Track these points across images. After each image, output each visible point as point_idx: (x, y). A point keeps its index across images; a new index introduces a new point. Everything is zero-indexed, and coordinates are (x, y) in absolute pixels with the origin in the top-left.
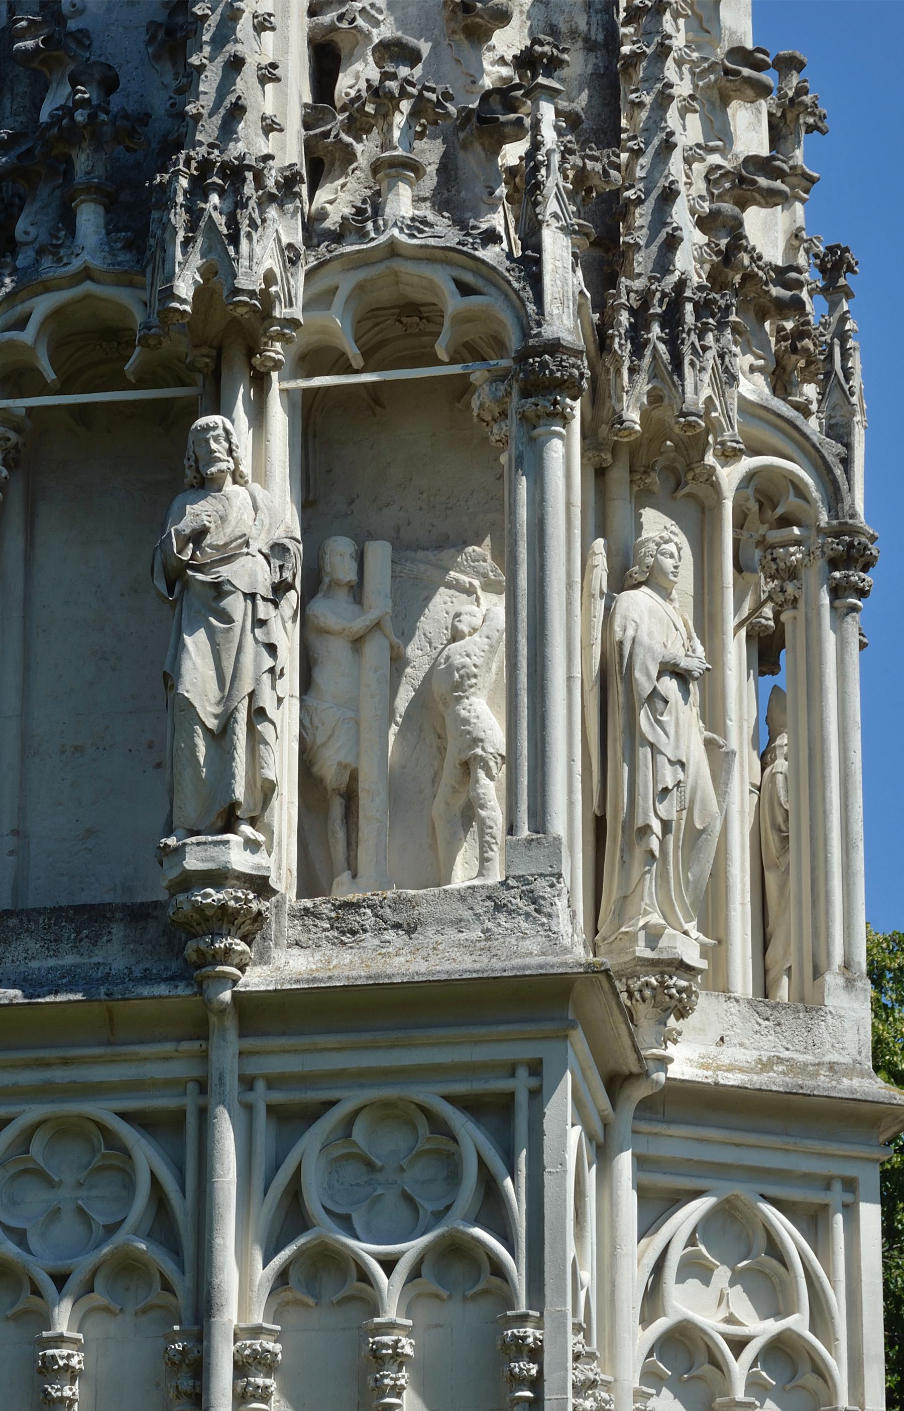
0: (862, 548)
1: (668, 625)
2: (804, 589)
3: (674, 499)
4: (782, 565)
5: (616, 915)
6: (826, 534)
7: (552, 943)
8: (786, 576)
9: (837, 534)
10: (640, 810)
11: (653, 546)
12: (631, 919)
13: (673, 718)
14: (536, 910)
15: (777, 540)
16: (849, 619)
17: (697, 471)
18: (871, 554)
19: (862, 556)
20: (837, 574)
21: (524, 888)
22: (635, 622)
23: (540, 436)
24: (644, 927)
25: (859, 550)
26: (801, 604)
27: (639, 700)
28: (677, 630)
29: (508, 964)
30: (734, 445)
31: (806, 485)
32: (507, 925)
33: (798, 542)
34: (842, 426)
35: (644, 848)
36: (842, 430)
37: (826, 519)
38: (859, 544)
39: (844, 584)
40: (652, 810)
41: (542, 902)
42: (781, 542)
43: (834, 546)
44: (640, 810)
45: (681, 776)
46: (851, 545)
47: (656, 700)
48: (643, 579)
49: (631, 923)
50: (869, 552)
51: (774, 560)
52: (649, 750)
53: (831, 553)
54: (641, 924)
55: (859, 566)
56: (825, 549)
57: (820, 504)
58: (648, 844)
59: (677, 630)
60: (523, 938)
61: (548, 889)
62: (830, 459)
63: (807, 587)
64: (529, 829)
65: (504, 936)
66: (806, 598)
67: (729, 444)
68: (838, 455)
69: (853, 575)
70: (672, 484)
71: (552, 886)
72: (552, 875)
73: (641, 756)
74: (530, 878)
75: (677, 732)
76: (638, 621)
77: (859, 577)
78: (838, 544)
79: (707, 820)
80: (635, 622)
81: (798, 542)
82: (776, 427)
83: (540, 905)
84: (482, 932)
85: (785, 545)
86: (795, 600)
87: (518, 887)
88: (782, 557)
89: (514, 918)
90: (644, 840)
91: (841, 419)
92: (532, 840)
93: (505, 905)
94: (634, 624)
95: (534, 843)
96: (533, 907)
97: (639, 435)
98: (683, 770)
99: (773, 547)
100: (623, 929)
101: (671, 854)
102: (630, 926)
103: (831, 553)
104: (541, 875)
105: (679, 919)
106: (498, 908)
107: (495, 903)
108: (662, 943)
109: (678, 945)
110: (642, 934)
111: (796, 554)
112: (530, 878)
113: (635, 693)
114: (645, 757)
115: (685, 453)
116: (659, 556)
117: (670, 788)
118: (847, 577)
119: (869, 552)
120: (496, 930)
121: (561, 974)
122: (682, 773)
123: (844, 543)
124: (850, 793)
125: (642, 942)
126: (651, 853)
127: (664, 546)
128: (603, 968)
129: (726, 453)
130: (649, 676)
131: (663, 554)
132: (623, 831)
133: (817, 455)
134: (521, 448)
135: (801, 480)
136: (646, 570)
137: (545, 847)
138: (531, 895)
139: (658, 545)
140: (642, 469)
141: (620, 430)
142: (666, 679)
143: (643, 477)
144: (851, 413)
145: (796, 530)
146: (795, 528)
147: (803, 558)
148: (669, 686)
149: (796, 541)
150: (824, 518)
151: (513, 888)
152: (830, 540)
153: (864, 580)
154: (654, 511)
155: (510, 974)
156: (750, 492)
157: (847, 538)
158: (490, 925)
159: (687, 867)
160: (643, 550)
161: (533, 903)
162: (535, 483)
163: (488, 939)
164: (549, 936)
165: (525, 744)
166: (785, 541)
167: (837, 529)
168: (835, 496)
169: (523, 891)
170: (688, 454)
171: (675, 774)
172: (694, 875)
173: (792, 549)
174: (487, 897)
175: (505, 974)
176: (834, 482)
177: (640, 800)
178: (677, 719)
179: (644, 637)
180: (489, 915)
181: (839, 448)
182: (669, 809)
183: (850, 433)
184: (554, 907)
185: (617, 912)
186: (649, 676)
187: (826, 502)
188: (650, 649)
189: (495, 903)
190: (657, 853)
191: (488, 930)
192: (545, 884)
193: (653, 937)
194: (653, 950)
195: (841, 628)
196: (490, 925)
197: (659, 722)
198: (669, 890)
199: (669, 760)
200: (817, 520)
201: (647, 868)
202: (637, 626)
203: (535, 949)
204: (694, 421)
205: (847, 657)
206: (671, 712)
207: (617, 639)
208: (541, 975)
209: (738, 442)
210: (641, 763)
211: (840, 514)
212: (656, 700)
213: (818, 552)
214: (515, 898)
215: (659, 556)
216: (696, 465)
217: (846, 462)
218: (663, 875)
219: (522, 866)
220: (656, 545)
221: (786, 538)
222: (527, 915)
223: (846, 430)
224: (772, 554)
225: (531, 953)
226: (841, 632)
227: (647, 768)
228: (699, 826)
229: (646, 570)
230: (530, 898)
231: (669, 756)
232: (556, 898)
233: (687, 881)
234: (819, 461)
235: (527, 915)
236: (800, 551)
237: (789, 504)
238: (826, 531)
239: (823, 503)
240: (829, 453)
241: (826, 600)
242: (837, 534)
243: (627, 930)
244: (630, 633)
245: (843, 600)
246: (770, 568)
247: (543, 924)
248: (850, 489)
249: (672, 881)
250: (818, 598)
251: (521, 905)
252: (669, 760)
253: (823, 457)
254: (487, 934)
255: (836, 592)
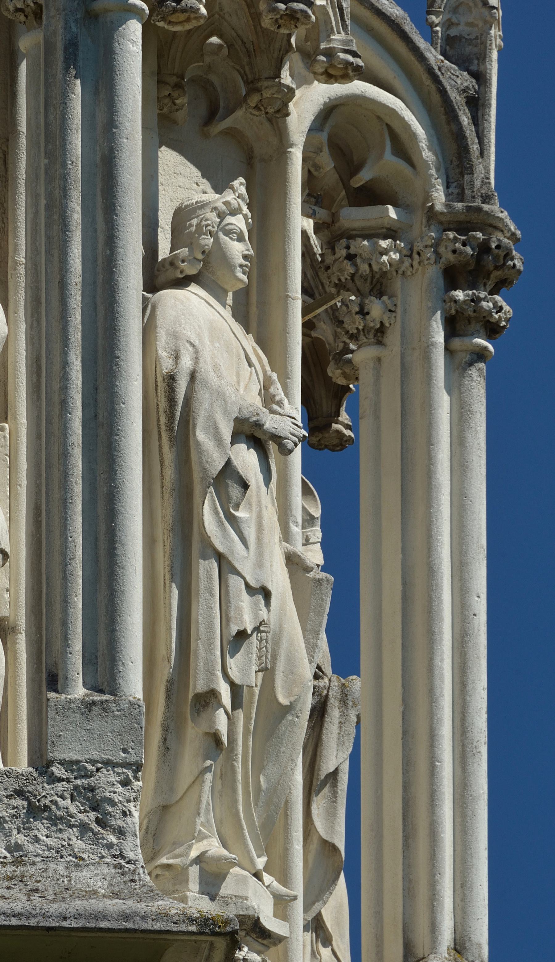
0: (502, 253)
1: (238, 356)
2: (399, 311)
3: (206, 136)
4: (364, 268)
5: (150, 836)
6: (441, 223)
7: (127, 878)
8: (366, 288)
9: (463, 227)
10: (199, 667)
11: (213, 217)
12: (176, 844)
13: (254, 515)
14: (98, 821)
15: (357, 225)
16: (474, 372)
17: (267, 94)
18: (514, 265)
19: (497, 268)
20: (460, 295)
21: (79, 782)
22: (192, 345)
23: (106, 11)
24: (199, 860)
25: (496, 258)
26: (393, 338)
27: (203, 479)
28: (250, 365)
29: (54, 908)
30: (350, 58)
31: (414, 136)
32: (49, 841)
33: (391, 233)
34: (470, 42)
35: (204, 727)
36: (469, 49)
37: (443, 198)
38: (498, 247)
39: (470, 312)
40: (220, 668)
41: (110, 809)
42: (363, 229)
43: (458, 245)
44: (201, 665)
45: (264, 614)
46: (484, 248)
47: (229, 482)
48: (192, 271)
49: (177, 851)
50: (510, 263)
51: (351, 257)
52: (215, 565)
53: (451, 257)
54: (194, 854)
55: (490, 285)
56: (442, 250)
57: (433, 171)
58: (212, 722)
59: (250, 365)
60: (77, 866)
61: (119, 788)
62: (455, 97)
63: (405, 311)
64: (85, 685)
65: (45, 859)
66: (403, 328)
67: (342, 55)
68: (464, 91)
69: (485, 299)
70: (203, 110)
71: (125, 783)
72: (126, 765)
73: (202, 574)
74: (89, 767)
75: (259, 540)
76: (197, 343)
77: (495, 303)
78: (464, 244)
79: (296, 691)
80: (192, 345)
81: (391, 233)
82: (370, 31)
83: (106, 814)
84: (8, 849)
85: (372, 234)
86: (381, 331)
87: (68, 780)
88: (365, 255)
89: (61, 831)
90: (204, 715)
91: (468, 29)
92: (94, 703)
93: (46, 808)
94: (191, 349)
95: (96, 709)
96: (92, 815)
97: (202, 21)
98: (268, 603)
99: (350, 235)
100: (164, 860)
101: (240, 742)
102: (176, 857)
103: (451, 257)
104: (108, 763)
105: (249, 852)
106: (36, 811)
107: (30, 803)
108: (227, 889)
109: (250, 894)
110: (194, 872)
111: (390, 252)
112: (89, 767)
113: (195, 467)
114: (210, 577)
115: (246, 60)
116: (221, 234)
117: (249, 632)
118: (476, 300)
119: (510, 263)
120: (31, 848)
121: (160, 932)
122: (264, 609)
123: (475, 243)
124: (470, 664)
125: (194, 885)
126: (216, 738)
127: (229, 219)
128: (229, 929)
129: (331, 71)
130: (218, 440)
131: (227, 233)
132: (168, 697)
133: (433, 88)
134: (74, 29)
135: (407, 126)
136: (200, 257)
137: (114, 717)
138: (90, 794)
139: (221, 216)
140: (174, 79)
141: (175, 10)
142: (242, 447)
143: (175, 94)
144: (486, 22)
145: (392, 213)
146: (390, 207)
147: (401, 261)
148: (246, 459)
149: (389, 229)
150: (439, 197)
151: (60, 780)
152: (451, 234)
153: (501, 308)
154: (174, 154)
155: (74, 925)
156: (323, 137)
157: (479, 235)
158: (21, 839)
159: (259, 768)
160: (195, 222)
161: (94, 809)
162: (96, 92)
163: (18, 862)
164: (121, 867)
165: (79, 539)
166: (370, 228)
167: (462, 218)
168: (458, 162)
169: (76, 788)
170: (250, 63)
171: (255, 609)
172: (268, 781)
173: (384, 244)
174: (15, 791)
175: (66, 924)
176: (459, 136)
177: (199, 647)
178: (260, 517)
179: (207, 370)
180: (18, 822)
181: (465, 80)
182: (243, 667)
183: (483, 57)
184: (128, 819)
185: (152, 830)
186: (218, 440)
187: (443, 170)
188: (220, 394)
189: (30, 803)
190: (225, 739)
191: (18, 847)
192: (114, 778)
193: (212, 879)
194: (213, 899)
195: (460, 385)
196: (21, 839)
197: (233, 520)
198: (235, 801)
199: (247, 585)
200: (428, 197)
201: (208, 763)
202: (196, 352)
203: (102, 886)
204: (302, 11)
205: (469, 436)
206: (250, 504)
207: (165, 371)
208: (127, 930)
209: (355, 54)
210: (201, 585)
211: (467, 192)
212: (229, 482)
213: (429, 254)
214: (63, 797)
215: (221, 234)
216: (266, 83)
217: (476, 104)
218: (227, 778)
219: (75, 745)
220: (219, 216)
221: (373, 223)
222: (84, 828)
223: (476, 50)
224: (348, 247)
225: (95, 892)
226: (460, 393)
227: (212, 595)
228: (283, 700)
229: (200, 257)
230: (88, 799)
231: (248, 579)
232: (132, 804)
233: (258, 789)
234: (436, 98)
235: (84, 828)
236: (396, 249)
237: (382, 166)
238: (443, 219)
239: (438, 170)
240: (452, 87)
241: (439, 336)
242: (463, 227)
243: (171, 861)
244: (186, 363)
245: (466, 340)
246: (341, 270)
247: (110, 846)
248: (482, 153)
249: (240, 787)
250: (426, 332)
251: (73, 809)
252: (247, 585)
253: (443, 92)
254: (16, 854)
255: (454, 326)
